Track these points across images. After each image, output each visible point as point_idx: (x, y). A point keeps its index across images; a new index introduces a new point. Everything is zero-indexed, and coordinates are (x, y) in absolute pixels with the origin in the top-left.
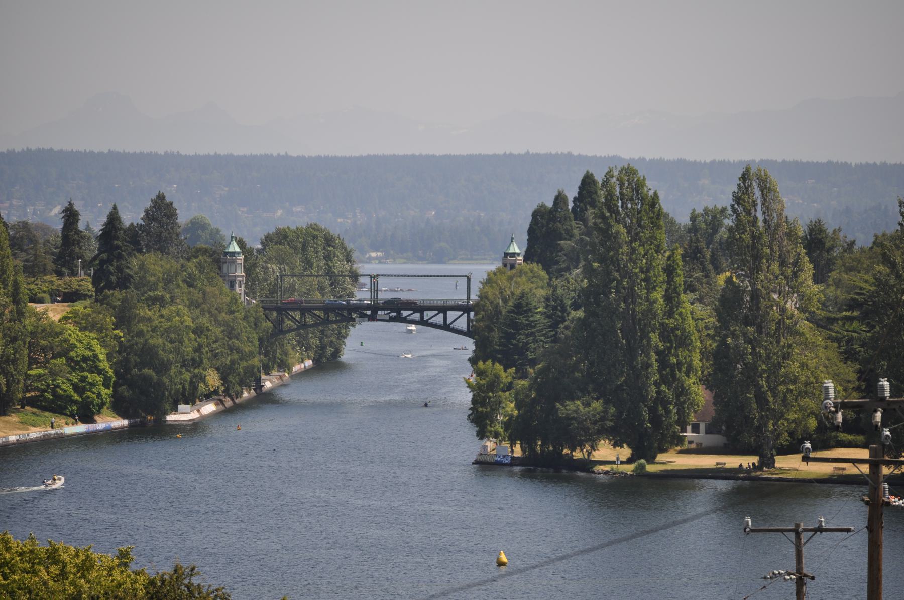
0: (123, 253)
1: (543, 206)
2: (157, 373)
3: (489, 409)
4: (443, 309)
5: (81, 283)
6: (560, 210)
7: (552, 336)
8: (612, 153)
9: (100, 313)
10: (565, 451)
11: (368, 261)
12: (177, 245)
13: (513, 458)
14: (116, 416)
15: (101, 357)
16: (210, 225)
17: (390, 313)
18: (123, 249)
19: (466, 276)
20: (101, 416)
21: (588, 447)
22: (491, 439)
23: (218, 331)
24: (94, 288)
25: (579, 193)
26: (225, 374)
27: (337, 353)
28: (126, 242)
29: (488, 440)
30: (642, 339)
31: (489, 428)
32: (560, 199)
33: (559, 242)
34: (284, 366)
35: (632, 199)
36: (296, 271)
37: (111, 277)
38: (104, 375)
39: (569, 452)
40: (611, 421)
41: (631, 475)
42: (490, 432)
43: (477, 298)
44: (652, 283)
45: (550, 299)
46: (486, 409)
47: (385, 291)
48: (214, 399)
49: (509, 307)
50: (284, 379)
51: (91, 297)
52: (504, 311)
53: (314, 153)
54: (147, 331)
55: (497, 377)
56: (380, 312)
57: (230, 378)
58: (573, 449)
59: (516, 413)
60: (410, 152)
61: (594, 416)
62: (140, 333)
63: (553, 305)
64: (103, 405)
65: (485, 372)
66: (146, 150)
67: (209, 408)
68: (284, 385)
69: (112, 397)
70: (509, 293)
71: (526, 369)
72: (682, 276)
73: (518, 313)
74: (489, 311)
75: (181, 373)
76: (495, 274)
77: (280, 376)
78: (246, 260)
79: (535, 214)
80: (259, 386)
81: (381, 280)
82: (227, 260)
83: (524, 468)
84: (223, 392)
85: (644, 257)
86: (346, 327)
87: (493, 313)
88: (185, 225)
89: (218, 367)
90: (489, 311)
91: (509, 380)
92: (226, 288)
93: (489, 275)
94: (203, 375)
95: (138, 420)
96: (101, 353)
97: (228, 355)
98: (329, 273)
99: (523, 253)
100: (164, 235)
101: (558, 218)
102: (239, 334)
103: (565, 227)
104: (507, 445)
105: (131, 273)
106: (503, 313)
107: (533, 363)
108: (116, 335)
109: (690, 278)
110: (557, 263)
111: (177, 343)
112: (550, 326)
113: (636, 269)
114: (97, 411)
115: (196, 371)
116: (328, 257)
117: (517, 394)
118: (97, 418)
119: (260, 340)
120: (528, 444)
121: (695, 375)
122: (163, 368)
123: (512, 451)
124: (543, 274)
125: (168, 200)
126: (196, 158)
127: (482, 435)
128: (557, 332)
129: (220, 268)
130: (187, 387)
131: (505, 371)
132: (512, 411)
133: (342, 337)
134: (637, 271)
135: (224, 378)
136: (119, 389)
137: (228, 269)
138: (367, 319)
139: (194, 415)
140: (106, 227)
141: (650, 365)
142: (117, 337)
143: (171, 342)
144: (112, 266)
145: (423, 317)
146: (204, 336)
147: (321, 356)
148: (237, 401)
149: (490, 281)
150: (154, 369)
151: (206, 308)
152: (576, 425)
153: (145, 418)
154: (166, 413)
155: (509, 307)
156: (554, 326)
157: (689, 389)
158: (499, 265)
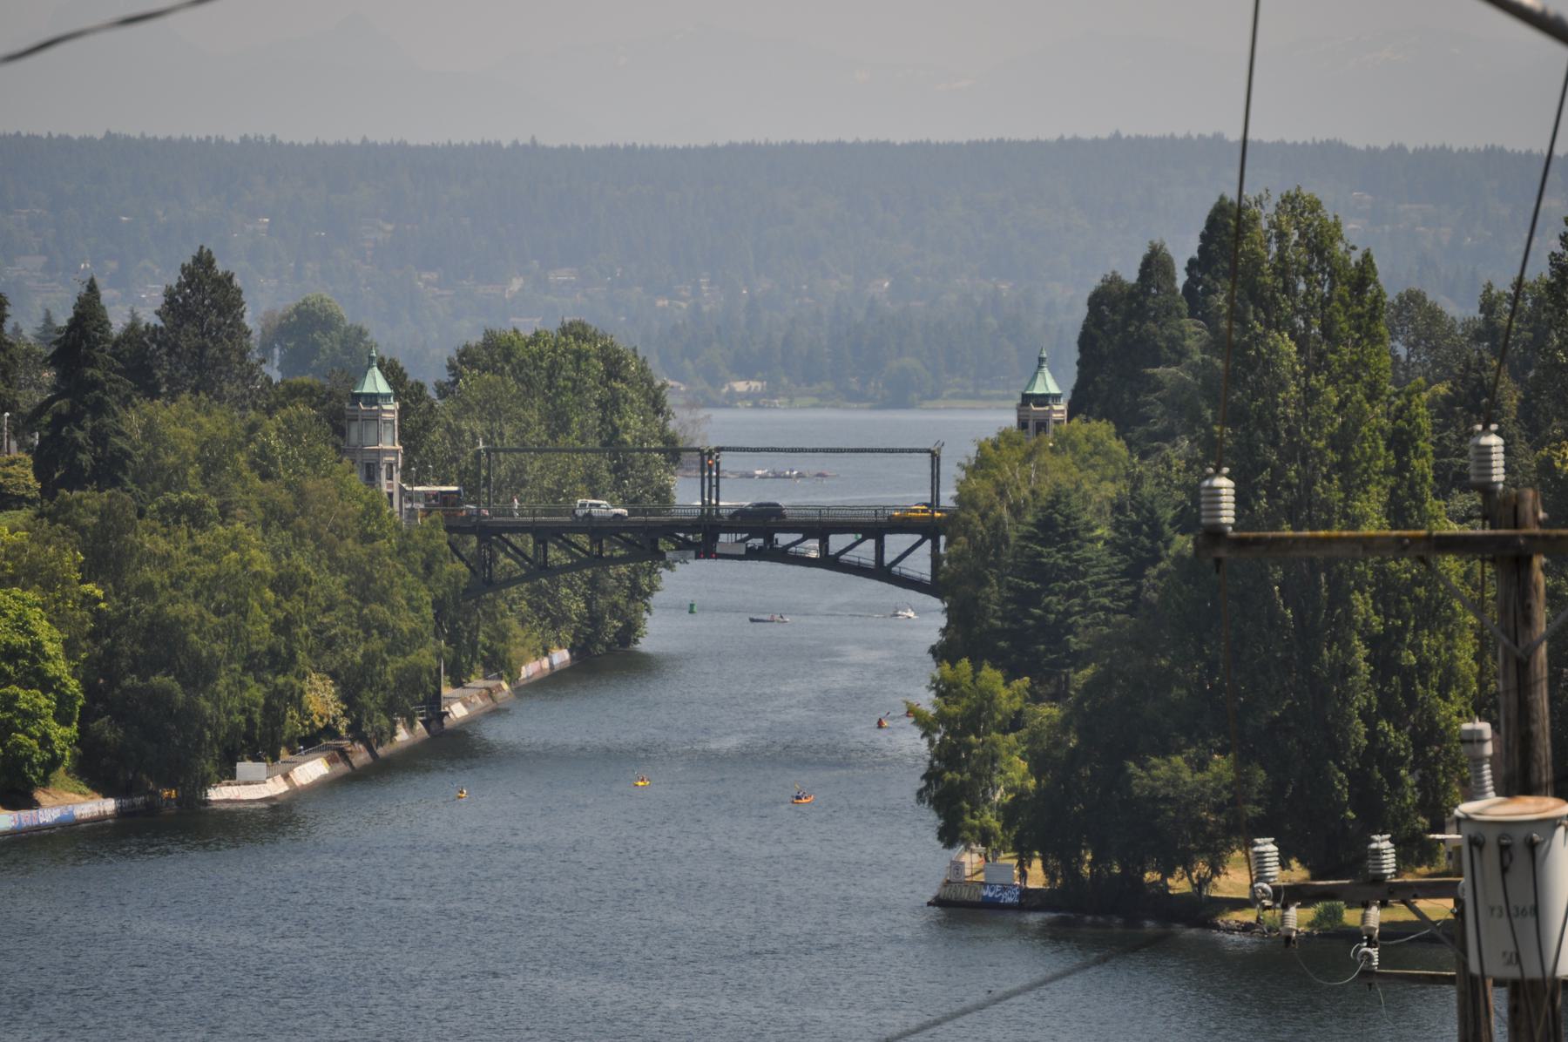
0: (107, 398)
1: (1113, 280)
2: (185, 686)
3: (967, 776)
4: (876, 528)
5: (10, 470)
6: (1154, 291)
7: (1127, 597)
8: (1321, 136)
9: (48, 542)
10: (1149, 876)
11: (727, 402)
12: (242, 378)
13: (1026, 893)
14: (88, 791)
15: (51, 648)
16: (341, 318)
17: (747, 539)
18: (107, 387)
19: (928, 451)
20: (50, 790)
21: (1202, 868)
22: (974, 847)
23: (336, 584)
24: (38, 481)
25: (1201, 250)
27: (630, 631)
28: (117, 371)
29: (967, 848)
30: (1332, 607)
31: (968, 819)
32: (1155, 264)
33: (1149, 371)
34: (498, 664)
35: (1308, 272)
36: (531, 438)
37: (81, 456)
38: (56, 692)
39: (1158, 877)
40: (1258, 803)
41: (1307, 934)
42: (972, 829)
43: (951, 504)
44: (1357, 476)
45: (1125, 507)
46: (962, 774)
47: (761, 477)
48: (327, 748)
49: (1025, 528)
50: (499, 696)
51: (31, 502)
52: (1013, 536)
53: (600, 141)
54: (163, 586)
55: (989, 698)
56: (723, 537)
57: (365, 697)
58: (1168, 872)
59: (1031, 783)
60: (831, 137)
61: (1216, 792)
62: (146, 590)
63: (1132, 522)
64: (53, 764)
65: (957, 686)
66: (197, 132)
67: (312, 770)
68: (496, 712)
69: (78, 743)
70: (1025, 492)
71: (1067, 676)
72: (1430, 455)
73: (1045, 542)
74: (979, 537)
75: (243, 686)
76: (995, 446)
77: (488, 689)
78: (404, 412)
79: (1098, 301)
80: (435, 714)
81: (726, 460)
82: (359, 414)
83: (1053, 915)
84: (349, 729)
85: (1337, 410)
86: (651, 572)
87: (987, 540)
88: (283, 317)
89: (336, 670)
90: (979, 537)
91: (1017, 704)
92: (356, 480)
93: (981, 449)
94: (297, 691)
95: (139, 800)
96: (50, 639)
97: (359, 641)
98: (612, 442)
99: (1067, 396)
100: (213, 351)
101: (1151, 309)
102: (385, 591)
103: (1167, 333)
104: (1009, 862)
105: (126, 447)
106: (1012, 541)
107: (1079, 660)
108: (86, 596)
109: (1460, 456)
110: (1144, 420)
111: (233, 614)
112: (1124, 574)
113: (1319, 439)
114: (39, 778)
115: (281, 680)
116: (610, 405)
117: (1034, 738)
118: (39, 795)
119: (439, 605)
120: (1059, 854)
121: (1463, 694)
122: (199, 674)
123: (1023, 875)
124: (1117, 446)
125: (220, 267)
126: (317, 151)
127: (950, 836)
128: (1140, 588)
129: (341, 431)
130: (258, 718)
131: (1007, 684)
132: (1024, 778)
133: (639, 593)
134: (1321, 444)
135: (349, 697)
136: (95, 725)
137: (360, 435)
138: (692, 553)
139: (275, 787)
140: (67, 337)
141: (1353, 671)
142: (88, 601)
143: (218, 612)
144: (82, 428)
145: (827, 547)
146: (297, 597)
147: (590, 641)
148: (381, 751)
149: (982, 464)
150: (177, 678)
151: (306, 527)
152: (1172, 814)
153: (155, 793)
154: (206, 783)
155: (1025, 528)
156: (1134, 572)
157: (1447, 727)
158: (1010, 419)
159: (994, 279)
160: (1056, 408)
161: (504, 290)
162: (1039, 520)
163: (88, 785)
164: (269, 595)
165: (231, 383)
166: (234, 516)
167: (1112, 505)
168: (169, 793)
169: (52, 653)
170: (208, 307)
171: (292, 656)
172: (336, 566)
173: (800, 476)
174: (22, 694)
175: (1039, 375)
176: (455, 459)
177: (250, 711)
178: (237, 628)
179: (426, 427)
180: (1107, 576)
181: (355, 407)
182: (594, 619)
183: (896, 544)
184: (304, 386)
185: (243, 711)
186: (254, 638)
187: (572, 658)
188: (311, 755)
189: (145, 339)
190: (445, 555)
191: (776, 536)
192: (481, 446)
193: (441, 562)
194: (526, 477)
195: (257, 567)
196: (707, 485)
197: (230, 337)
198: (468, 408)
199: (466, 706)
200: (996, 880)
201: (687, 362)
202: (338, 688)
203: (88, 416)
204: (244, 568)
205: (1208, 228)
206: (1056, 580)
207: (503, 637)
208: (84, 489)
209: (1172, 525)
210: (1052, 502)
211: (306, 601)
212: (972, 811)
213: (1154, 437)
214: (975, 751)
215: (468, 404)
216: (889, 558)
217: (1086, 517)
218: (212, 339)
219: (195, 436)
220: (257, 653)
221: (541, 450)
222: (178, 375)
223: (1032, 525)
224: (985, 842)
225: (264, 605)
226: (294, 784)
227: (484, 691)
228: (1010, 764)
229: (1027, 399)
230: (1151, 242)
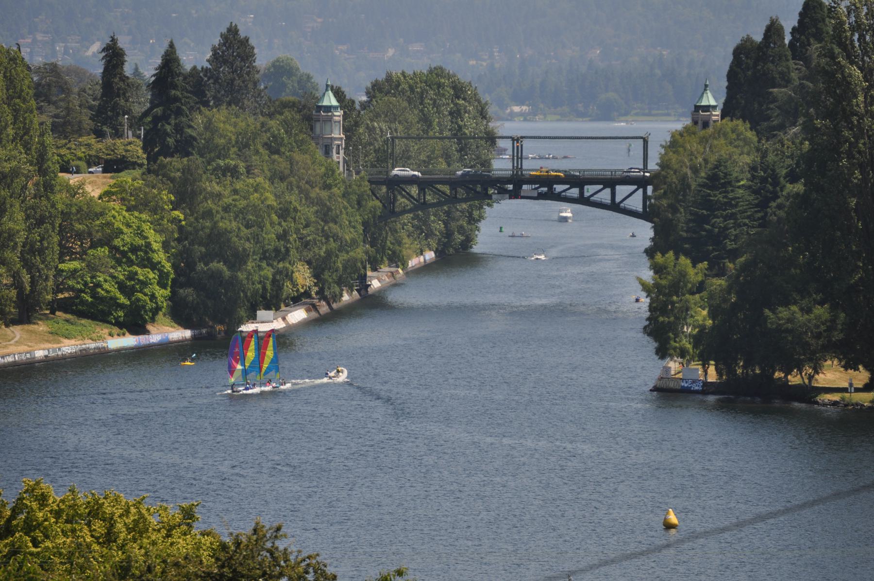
1: (748, 40)
3: (672, 319)
4: (611, 183)
5: (129, 148)
6: (772, 45)
7: (759, 219)
11: (509, 118)
13: (706, 384)
15: (155, 246)
16: (298, 69)
19: (642, 138)
20: (155, 325)
23: (308, 212)
25: (800, 22)
26: (318, 270)
27: (468, 242)
28: (188, 92)
31: (672, 343)
32: (773, 30)
33: (771, 90)
34: (397, 259)
37: (168, 139)
38: (159, 270)
42: (675, 349)
46: (669, 318)
47: (532, 158)
48: (305, 304)
49: (701, 180)
50: (398, 276)
52: (693, 186)
55: (683, 275)
56: (525, 187)
58: (788, 372)
61: (817, 327)
62: (208, 214)
64: (157, 309)
67: (298, 315)
70: (700, 160)
71: (724, 264)
73: (713, 188)
74: (674, 185)
76: (681, 135)
77: (392, 273)
78: (345, 116)
79: (738, 52)
80: (364, 286)
83: (721, 397)
84: (317, 293)
87: (679, 187)
89: (310, 260)
90: (674, 185)
91: (700, 278)
92: (319, 154)
93: (673, 136)
95: (204, 331)
96: (155, 240)
97: (322, 244)
98: (458, 134)
99: (721, 106)
100: (237, 82)
101: (770, 56)
105: (194, 134)
107: (733, 255)
112: (757, 206)
115: (281, 265)
116: (456, 114)
117: (711, 297)
118: (149, 327)
119: (365, 224)
120: (725, 365)
122: (237, 260)
124: (750, 135)
125: (242, 34)
127: (663, 352)
128: (766, 214)
130: (269, 287)
131: (694, 266)
132: (704, 320)
133: (473, 220)
135: (317, 275)
137: (321, 129)
138: (507, 196)
139: (278, 325)
143: (247, 226)
144: (169, 124)
146: (290, 220)
148: (335, 306)
150: (225, 263)
153: (212, 327)
154: (241, 322)
156: (763, 205)
158: (688, 122)
159: (659, 48)
160: (714, 113)
161: (384, 55)
162: (709, 175)
163: (176, 323)
164: (275, 218)
165: (249, 100)
166: (253, 174)
167: (750, 167)
168: (219, 327)
169: (156, 248)
170: (235, 57)
171: (287, 250)
172: (311, 202)
173: (553, 158)
174: (139, 270)
175: (705, 95)
176: (371, 144)
177: (264, 282)
178: (257, 235)
179: (357, 124)
180: (747, 207)
181: (318, 114)
182: (449, 234)
183: (622, 191)
184: (290, 102)
185: (260, 282)
186: (266, 242)
187: (436, 256)
188: (298, 307)
189: (201, 74)
190: (368, 196)
191: (555, 186)
192: (389, 136)
193: (366, 200)
194: (410, 153)
195: (269, 202)
196: (520, 155)
197: (248, 73)
198: (377, 116)
199: (379, 281)
200: (689, 377)
201: (487, 95)
202: (311, 270)
203: (173, 117)
204: (262, 203)
205: (803, 9)
206: (718, 209)
207: (400, 243)
208: (173, 156)
209: (785, 178)
210: (716, 165)
211: (295, 222)
212: (675, 338)
213: (774, 128)
214: (676, 305)
215: (378, 113)
216: (618, 199)
217: (735, 175)
218: (238, 75)
219: (233, 130)
220: (268, 250)
221: (419, 138)
222: (219, 96)
223: (705, 178)
224: (683, 356)
225: (272, 224)
226: (288, 323)
227: (389, 274)
228: (696, 312)
229: (698, 108)
230: (771, 18)
